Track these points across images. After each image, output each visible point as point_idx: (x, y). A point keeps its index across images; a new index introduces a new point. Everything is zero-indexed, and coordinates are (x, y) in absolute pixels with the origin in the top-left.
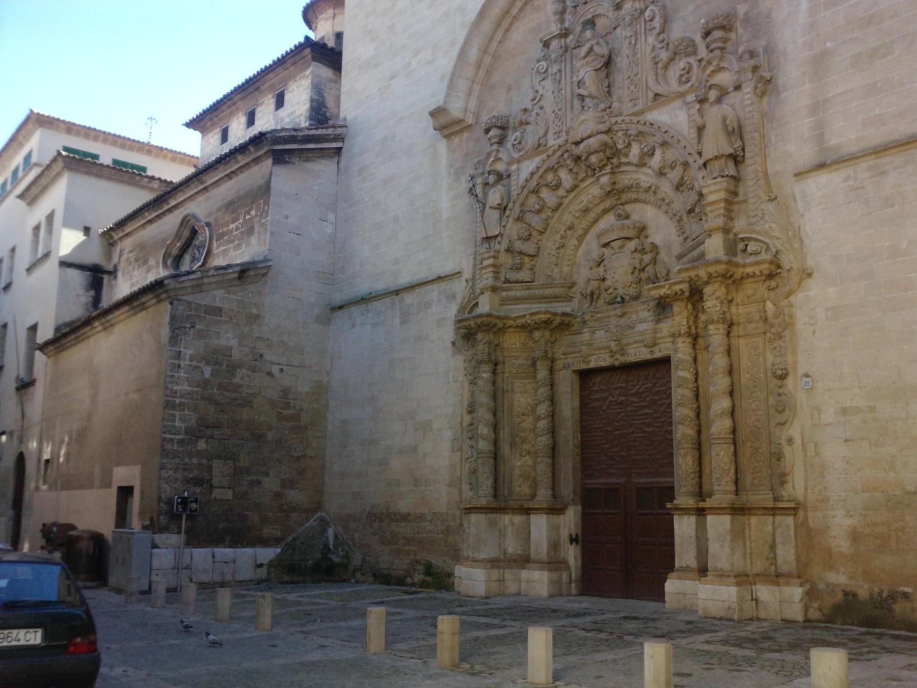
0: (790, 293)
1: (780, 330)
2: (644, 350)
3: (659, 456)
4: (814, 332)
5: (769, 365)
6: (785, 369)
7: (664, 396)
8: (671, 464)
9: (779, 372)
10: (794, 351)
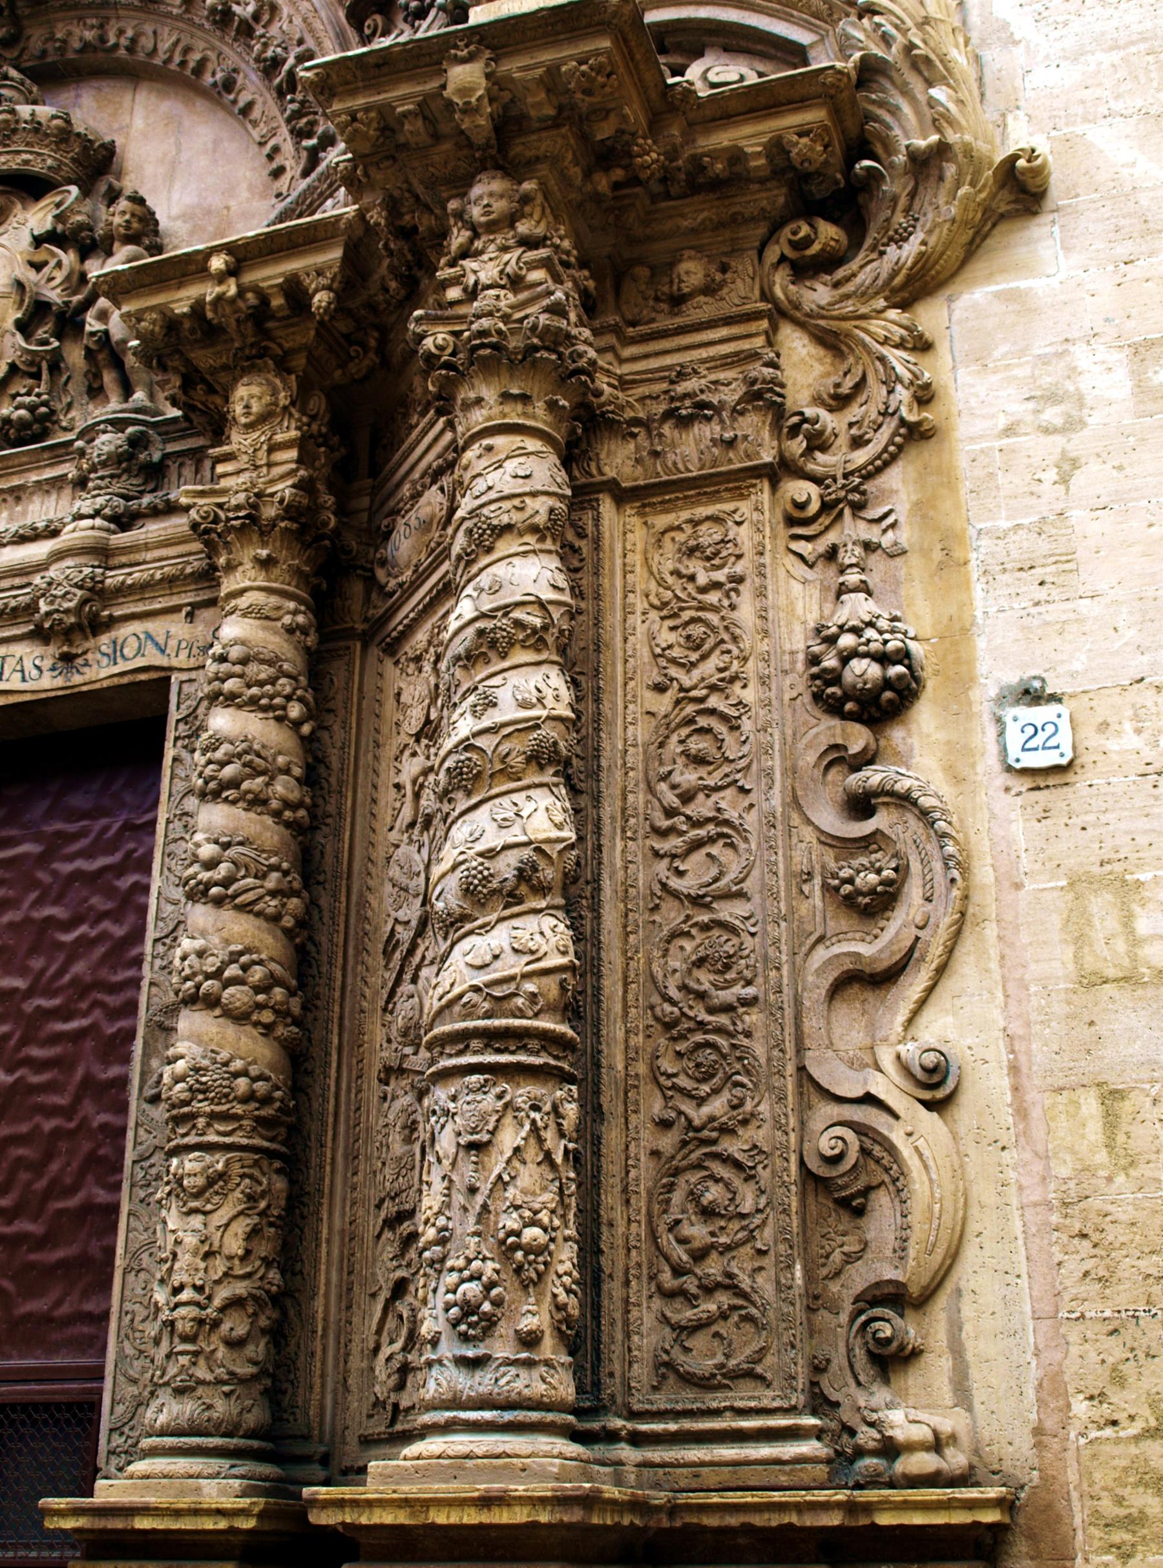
0: (918, 286)
1: (861, 457)
2: (28, 654)
3: (25, 1226)
4: (1068, 467)
5: (798, 641)
6: (904, 656)
7: (98, 902)
8: (97, 1272)
9: (864, 670)
10: (949, 561)
